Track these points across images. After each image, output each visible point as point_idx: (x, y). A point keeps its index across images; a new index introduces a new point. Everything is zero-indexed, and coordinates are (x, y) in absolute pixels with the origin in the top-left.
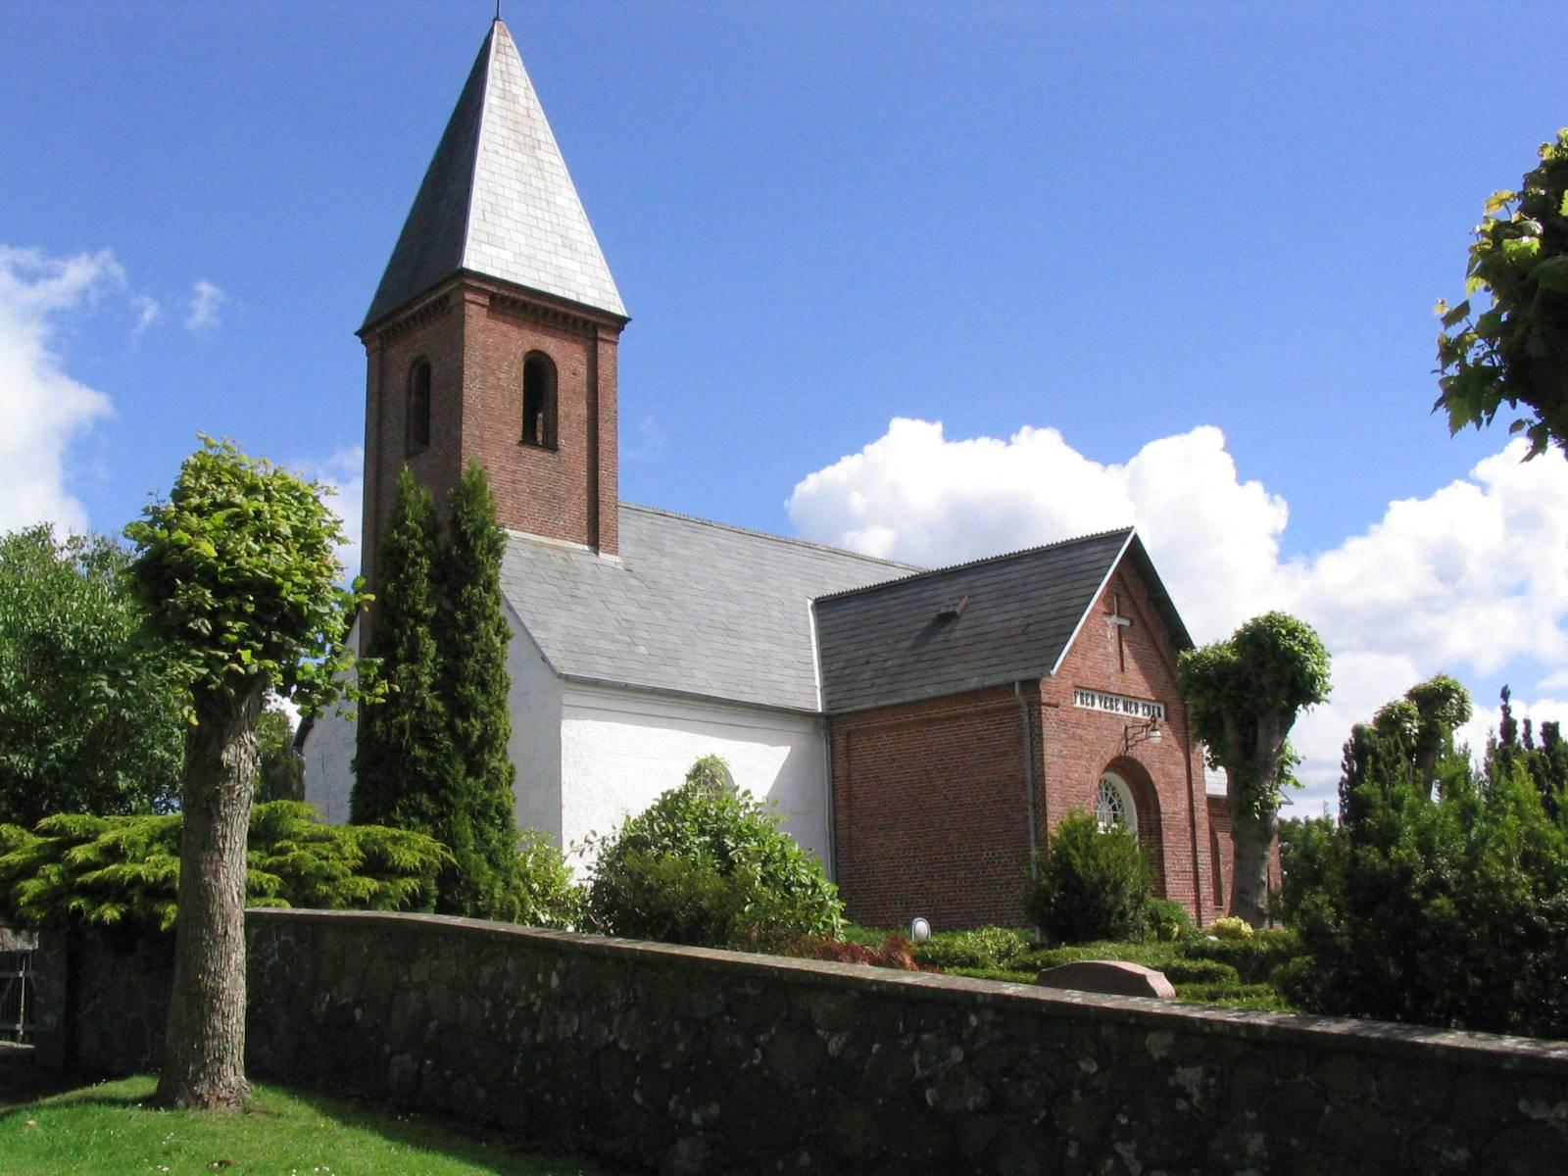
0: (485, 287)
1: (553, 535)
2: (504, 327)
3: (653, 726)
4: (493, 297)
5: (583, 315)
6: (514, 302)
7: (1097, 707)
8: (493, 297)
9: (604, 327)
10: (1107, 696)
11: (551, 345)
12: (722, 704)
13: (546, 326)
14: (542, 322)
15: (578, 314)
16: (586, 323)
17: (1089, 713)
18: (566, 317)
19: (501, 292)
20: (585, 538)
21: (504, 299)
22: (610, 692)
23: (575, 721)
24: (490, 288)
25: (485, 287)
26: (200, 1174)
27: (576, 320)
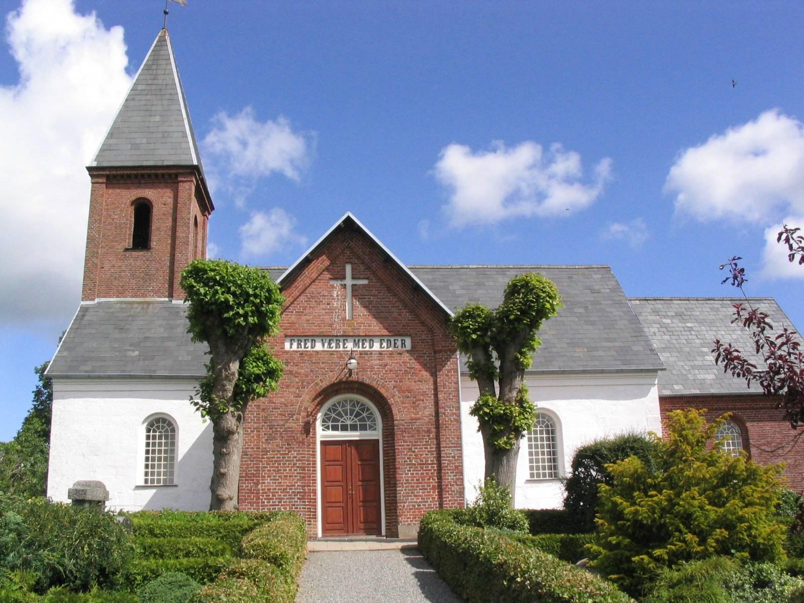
0: (102, 173)
1: (144, 296)
2: (118, 191)
3: (95, 397)
4: (108, 177)
5: (153, 171)
6: (122, 176)
7: (319, 347)
8: (108, 177)
9: (182, 174)
10: (358, 338)
11: (149, 193)
12: (186, 379)
13: (146, 183)
14: (142, 181)
15: (163, 172)
16: (170, 175)
17: (310, 355)
18: (156, 175)
19: (112, 173)
20: (167, 294)
21: (115, 176)
22: (140, 380)
23: (61, 400)
24: (104, 173)
25: (102, 173)
26: (444, 602)
27: (163, 175)
